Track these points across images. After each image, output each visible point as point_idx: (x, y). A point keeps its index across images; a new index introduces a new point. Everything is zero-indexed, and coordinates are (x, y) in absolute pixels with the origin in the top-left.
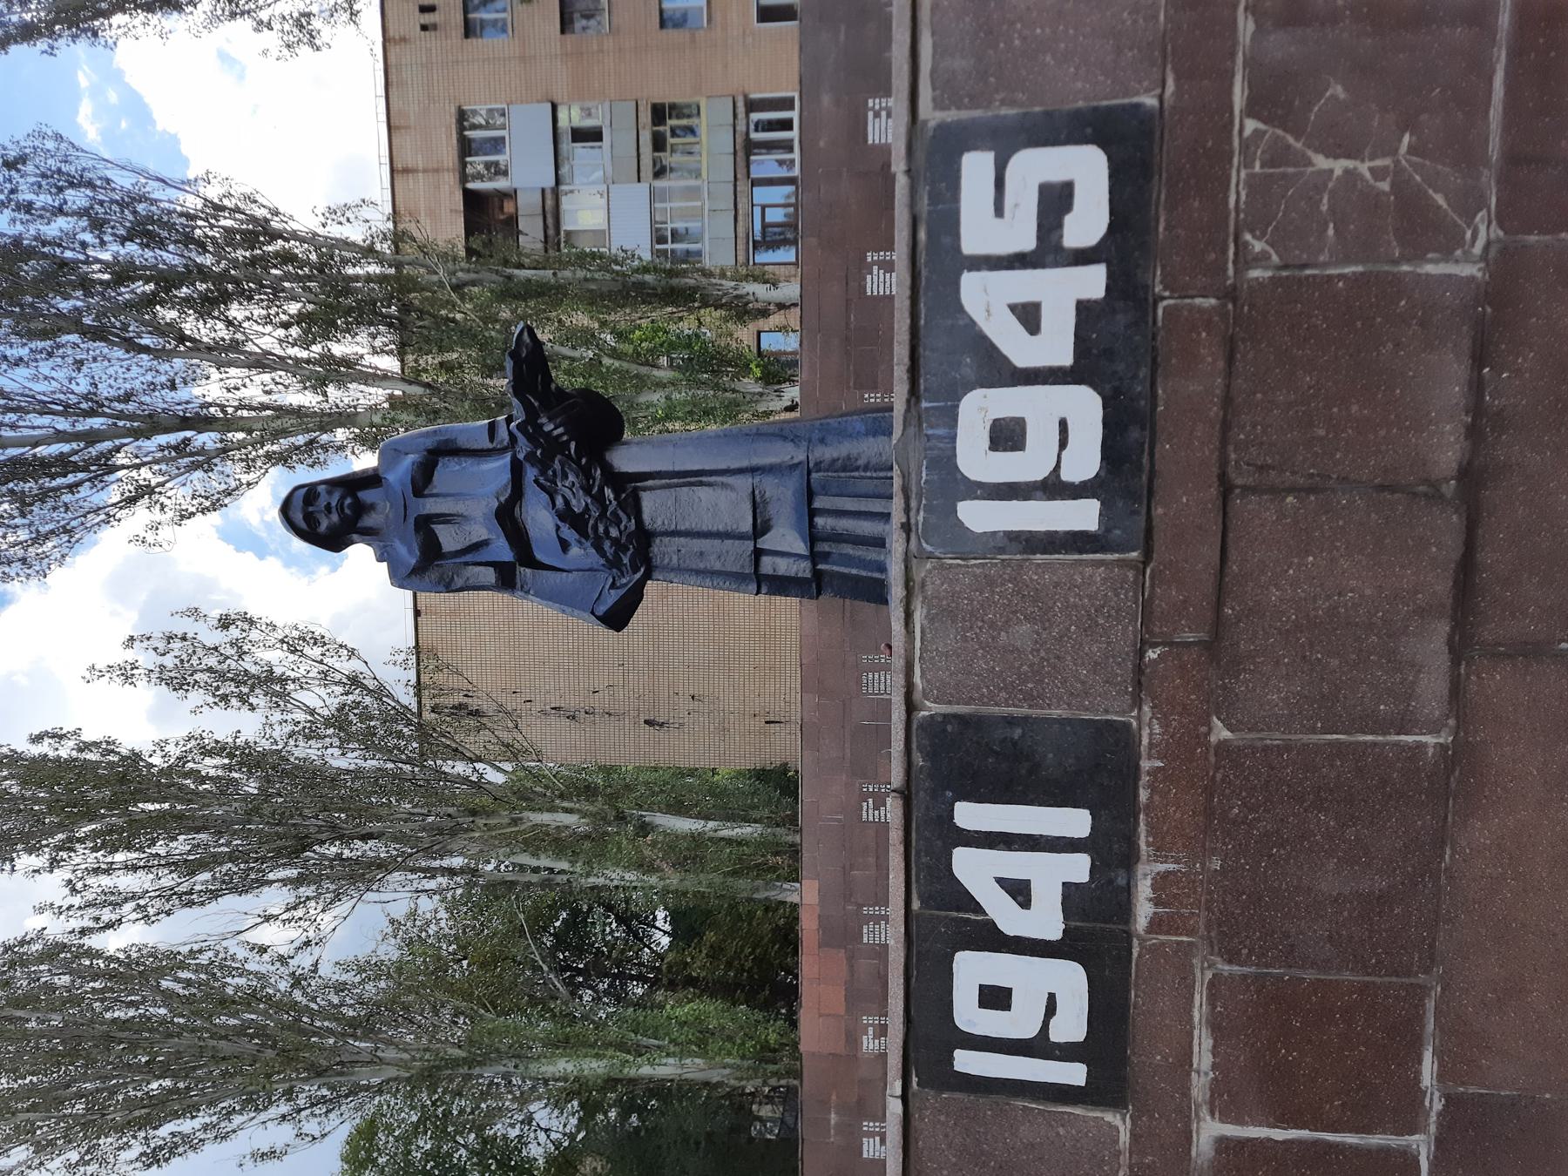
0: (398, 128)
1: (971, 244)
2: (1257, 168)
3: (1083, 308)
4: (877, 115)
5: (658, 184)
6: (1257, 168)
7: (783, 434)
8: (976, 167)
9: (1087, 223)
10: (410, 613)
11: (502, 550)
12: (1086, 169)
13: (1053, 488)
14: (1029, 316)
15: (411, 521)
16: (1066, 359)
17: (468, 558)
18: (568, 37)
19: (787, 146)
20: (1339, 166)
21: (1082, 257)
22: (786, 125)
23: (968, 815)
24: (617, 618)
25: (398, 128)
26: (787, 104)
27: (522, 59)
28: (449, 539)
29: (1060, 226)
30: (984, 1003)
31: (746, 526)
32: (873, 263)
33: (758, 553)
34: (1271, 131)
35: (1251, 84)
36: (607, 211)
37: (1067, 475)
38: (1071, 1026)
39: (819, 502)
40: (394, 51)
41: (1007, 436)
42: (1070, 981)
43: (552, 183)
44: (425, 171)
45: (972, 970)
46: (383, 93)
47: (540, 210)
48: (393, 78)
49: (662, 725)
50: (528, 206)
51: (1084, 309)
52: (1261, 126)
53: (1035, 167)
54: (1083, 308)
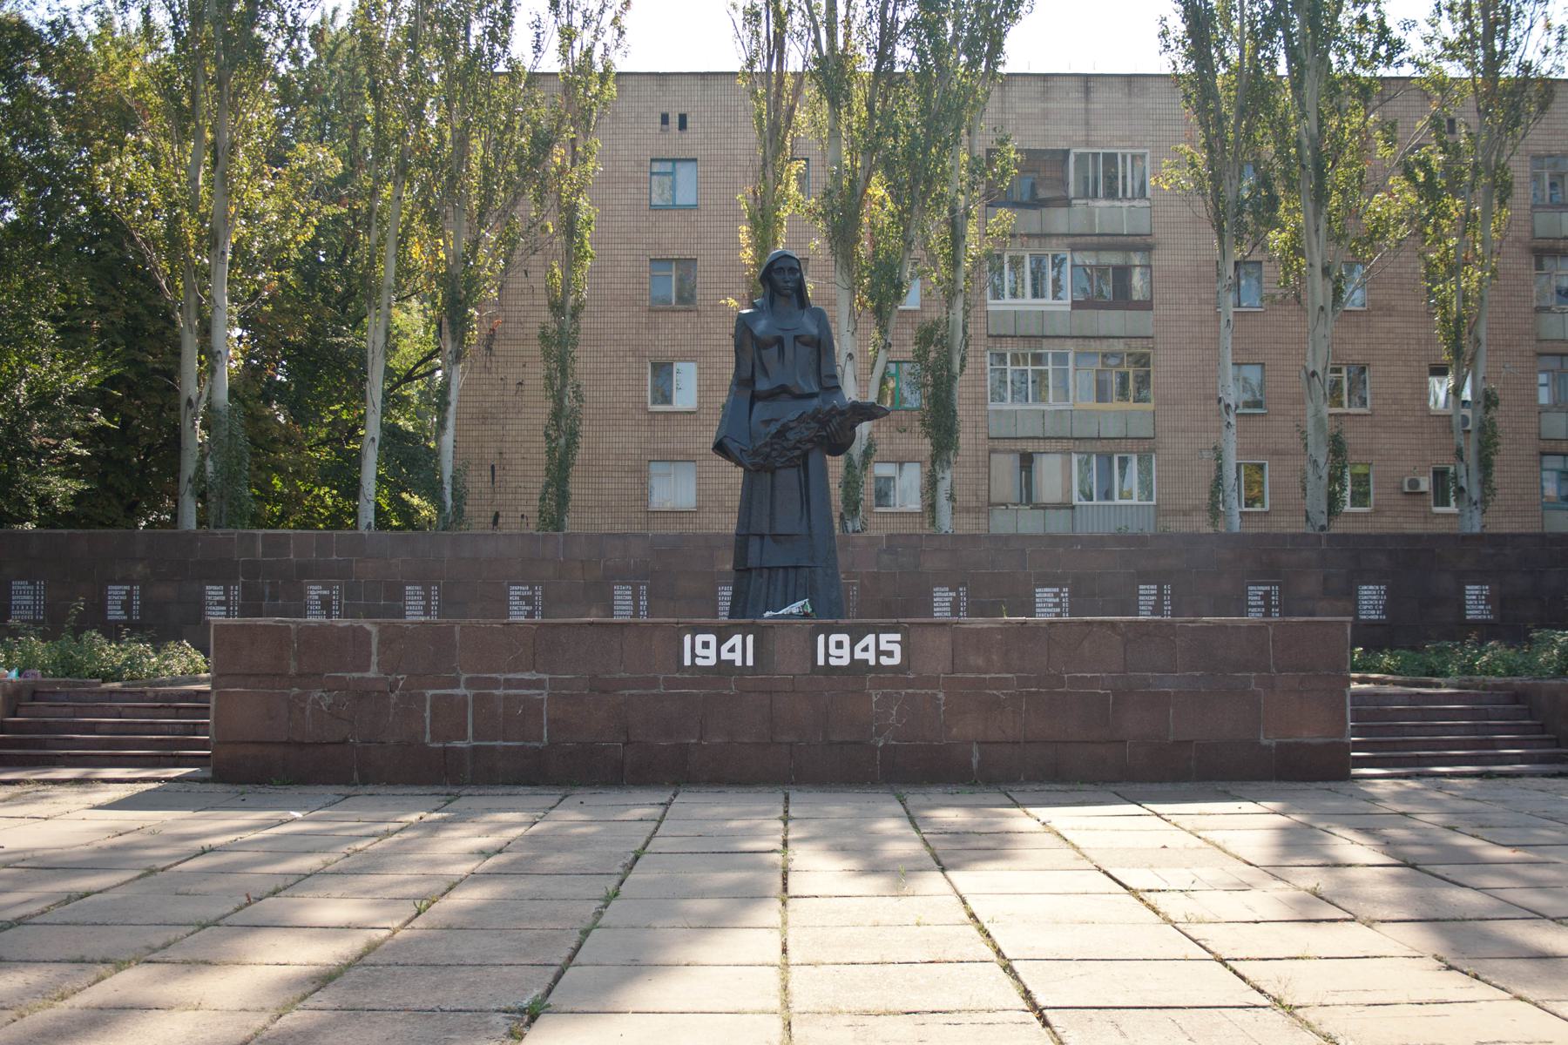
4: (1056, 595)
7: (768, 90)
8: (898, 637)
9: (884, 661)
11: (763, 385)
12: (896, 660)
13: (827, 655)
14: (866, 649)
15: (780, 333)
23: (750, 638)
24: (720, 448)
28: (771, 354)
31: (780, 529)
32: (958, 593)
33: (762, 536)
39: (792, 573)
41: (839, 645)
44: (1087, 110)
45: (712, 639)
47: (1046, 231)
49: (489, 347)
53: (897, 649)
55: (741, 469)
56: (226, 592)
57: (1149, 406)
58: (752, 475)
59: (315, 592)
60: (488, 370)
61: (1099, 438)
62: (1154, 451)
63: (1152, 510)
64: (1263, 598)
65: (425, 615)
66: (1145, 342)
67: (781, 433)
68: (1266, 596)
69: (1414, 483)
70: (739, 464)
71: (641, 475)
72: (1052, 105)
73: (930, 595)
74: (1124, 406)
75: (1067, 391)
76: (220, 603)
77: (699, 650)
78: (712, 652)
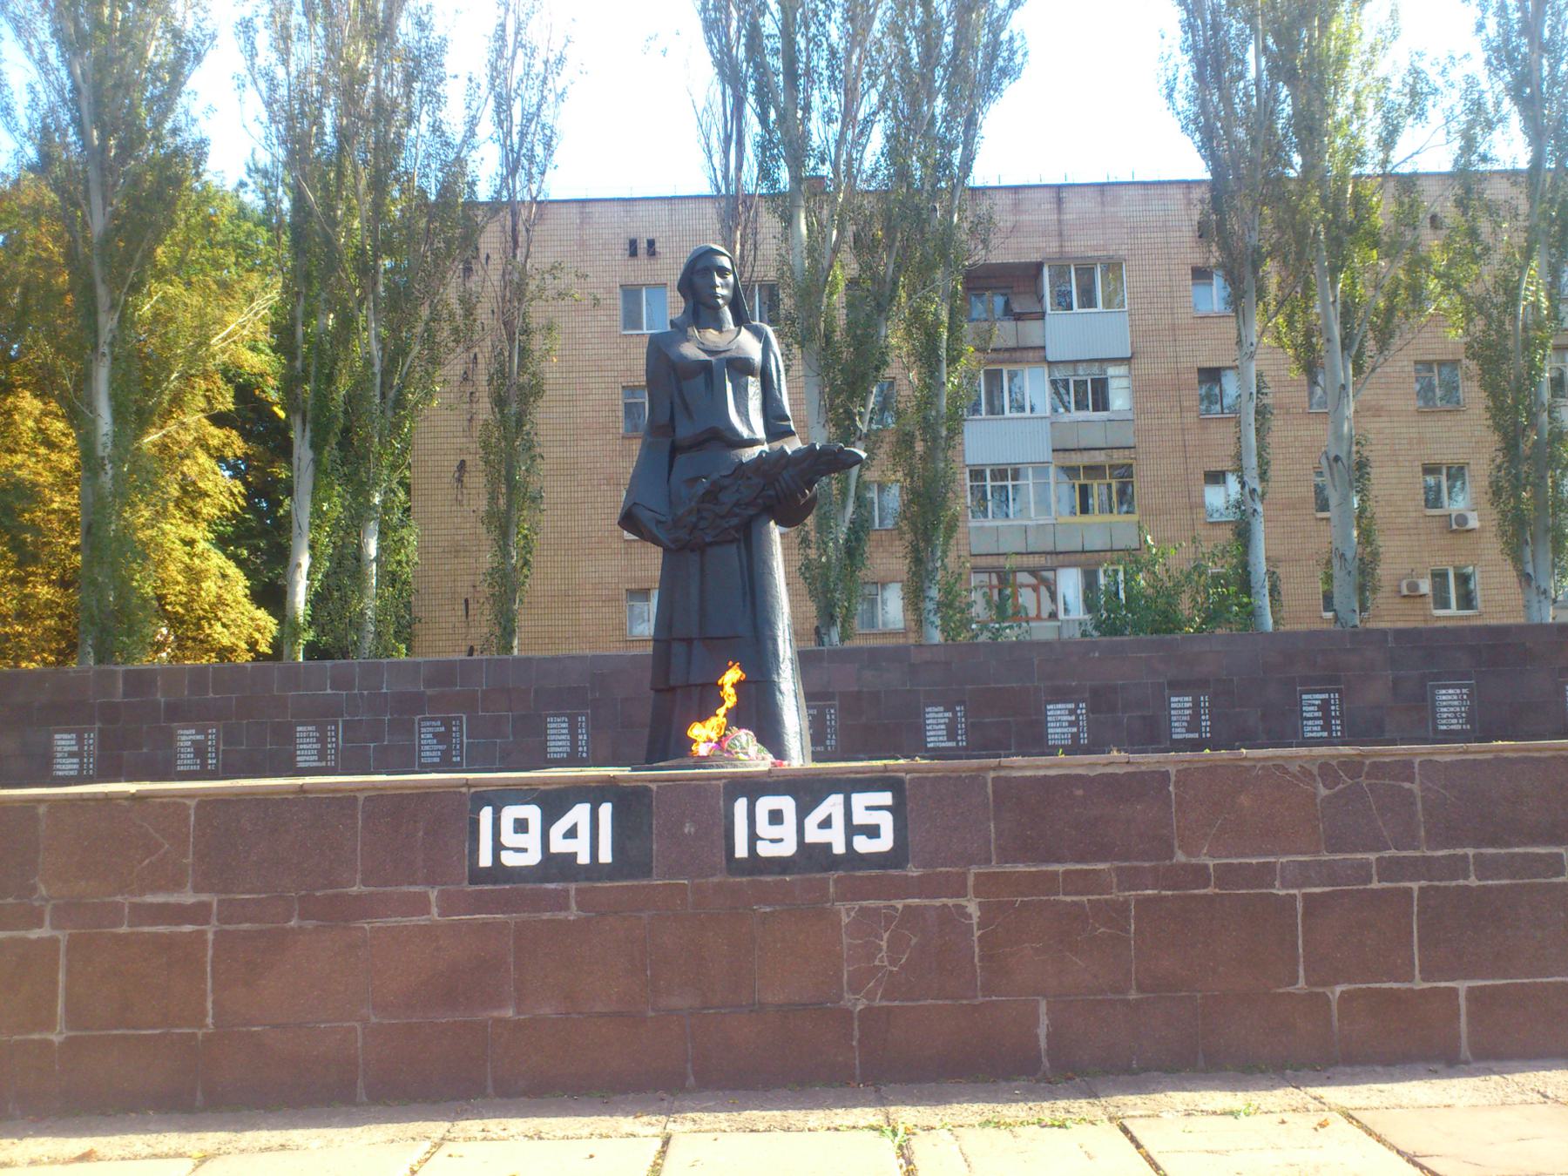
0: (1102, 194)
4: (1071, 712)
5: (1052, 470)
8: (886, 798)
9: (863, 845)
11: (685, 431)
12: (885, 843)
14: (826, 824)
17: (677, 400)
18: (1195, 376)
20: (884, 944)
21: (849, 843)
23: (606, 810)
24: (629, 520)
25: (1102, 194)
27: (1173, 328)
30: (516, 820)
32: (954, 713)
33: (689, 641)
36: (1015, 431)
37: (759, 843)
40: (1178, 193)
42: (533, 857)
43: (1050, 358)
44: (1060, 221)
45: (533, 813)
46: (1137, 179)
47: (1022, 344)
49: (460, 480)
50: (1031, 332)
51: (829, 846)
53: (886, 821)
56: (80, 741)
57: (1135, 518)
58: (674, 553)
59: (187, 737)
60: (460, 503)
61: (1083, 552)
64: (1320, 708)
66: (1127, 452)
67: (712, 495)
68: (1324, 706)
69: (1413, 587)
72: (1025, 218)
73: (920, 715)
74: (1106, 518)
75: (1049, 507)
76: (71, 755)
77: (508, 837)
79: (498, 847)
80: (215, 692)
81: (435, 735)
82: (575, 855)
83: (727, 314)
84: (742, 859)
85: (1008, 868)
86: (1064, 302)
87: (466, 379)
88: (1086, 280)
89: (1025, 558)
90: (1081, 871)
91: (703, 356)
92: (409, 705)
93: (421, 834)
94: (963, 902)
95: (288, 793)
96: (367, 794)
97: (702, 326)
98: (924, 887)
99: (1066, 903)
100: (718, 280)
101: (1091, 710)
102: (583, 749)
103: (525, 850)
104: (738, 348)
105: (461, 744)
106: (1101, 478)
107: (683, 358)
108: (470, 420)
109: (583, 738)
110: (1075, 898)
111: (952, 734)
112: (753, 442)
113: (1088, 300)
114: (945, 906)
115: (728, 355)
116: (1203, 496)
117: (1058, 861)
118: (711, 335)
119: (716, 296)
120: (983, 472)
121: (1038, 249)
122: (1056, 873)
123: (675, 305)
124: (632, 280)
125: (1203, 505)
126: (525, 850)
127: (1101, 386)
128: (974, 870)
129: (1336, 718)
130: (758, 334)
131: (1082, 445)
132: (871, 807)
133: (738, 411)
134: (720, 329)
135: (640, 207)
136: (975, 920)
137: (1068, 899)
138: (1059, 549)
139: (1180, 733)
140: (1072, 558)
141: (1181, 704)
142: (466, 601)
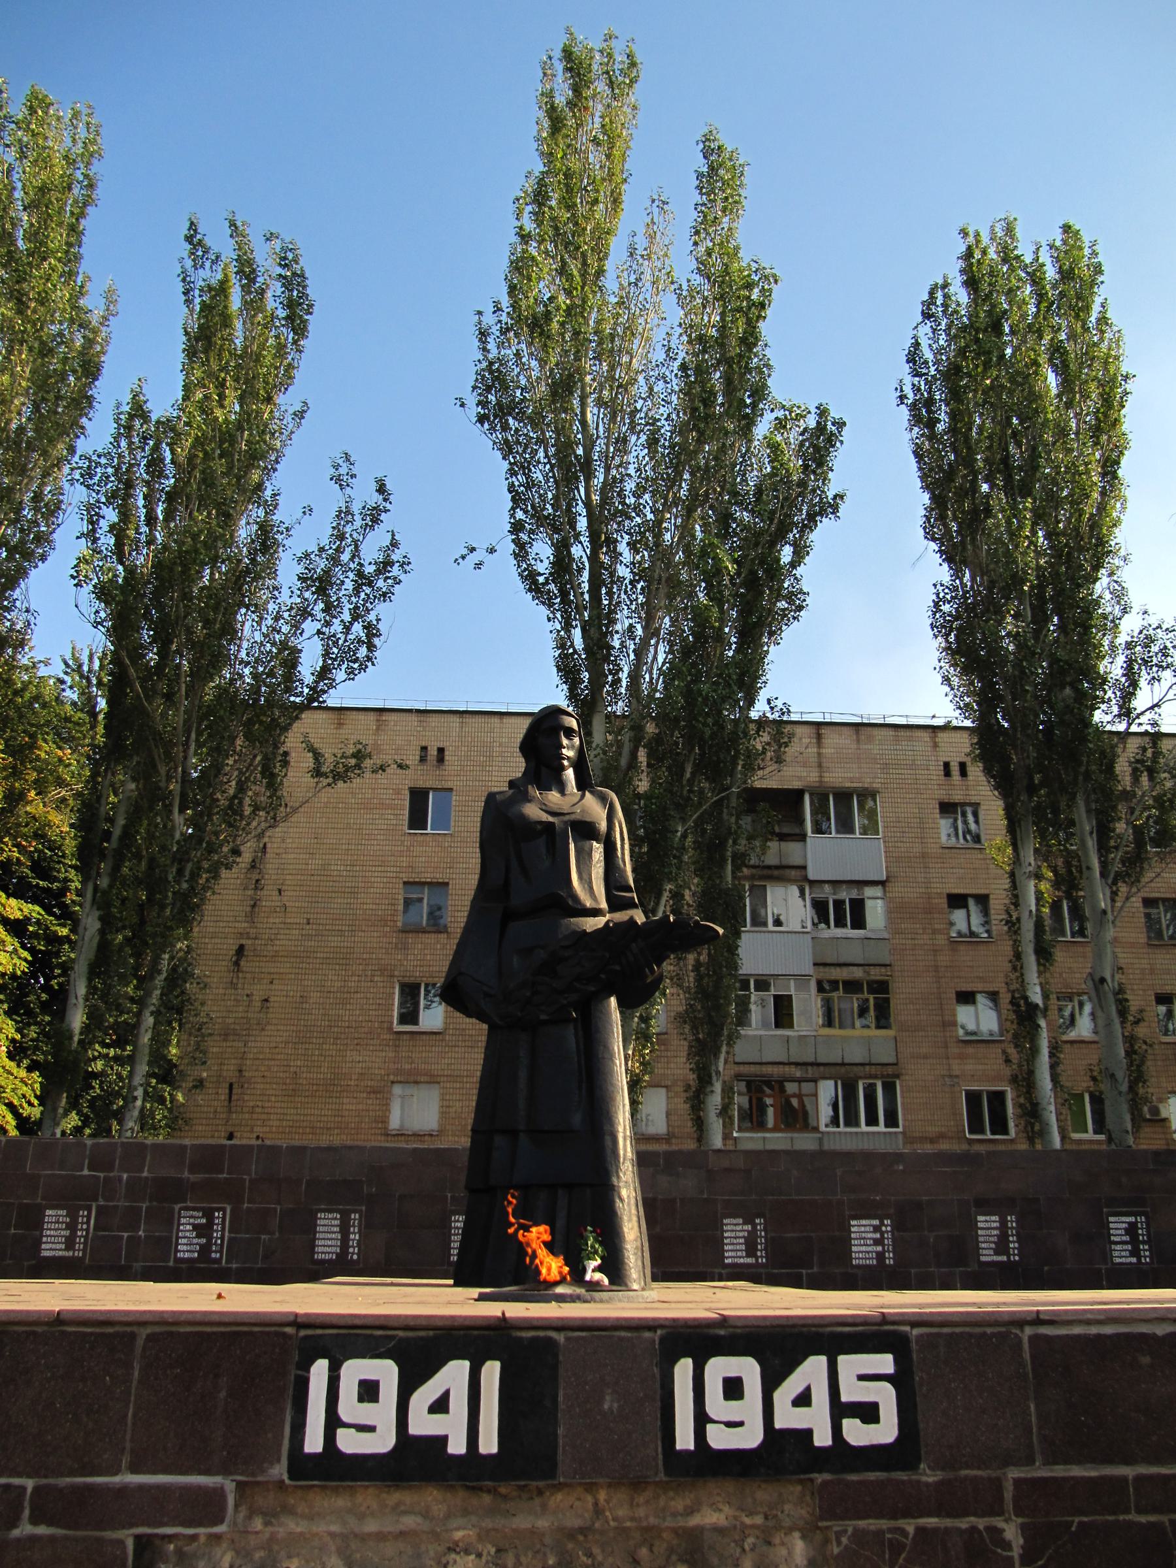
1: (842, 1359)
2: (888, 1536)
3: (809, 1433)
4: (876, 1229)
6: (888, 1536)
8: (885, 1363)
9: (856, 1433)
10: (379, 704)
12: (885, 1431)
13: (702, 1419)
14: (803, 1400)
16: (778, 1425)
19: (851, 1120)
22: (872, 1120)
23: (492, 1371)
25: (857, 733)
26: (891, 1120)
27: (924, 855)
29: (853, 1417)
30: (363, 1383)
32: (754, 1225)
34: (908, 1542)
35: (935, 1530)
38: (349, 1442)
41: (733, 1389)
42: (383, 1442)
44: (819, 754)
45: (386, 1372)
47: (784, 863)
48: (902, 733)
49: (237, 964)
50: (792, 852)
52: (911, 1536)
53: (886, 1396)
54: (809, 1433)
55: (485, 1026)
60: (233, 985)
62: (898, 1076)
63: (900, 1137)
65: (67, 1249)
66: (883, 970)
68: (1132, 1230)
70: (482, 1017)
71: (380, 1093)
73: (719, 1227)
78: (383, 1413)
79: (333, 1422)
80: (90, 1169)
81: (196, 1227)
82: (444, 1439)
83: (570, 774)
84: (686, 1452)
85: (1059, 1471)
86: (818, 830)
87: (253, 867)
88: (844, 806)
89: (787, 1068)
90: (1159, 1476)
91: (546, 817)
92: (168, 1194)
93: (223, 1394)
94: (998, 1522)
95: (36, 1323)
96: (149, 1330)
97: (544, 787)
98: (947, 1500)
99: (1140, 1524)
100: (565, 742)
101: (897, 1227)
102: (354, 1252)
103: (371, 1429)
104: (583, 811)
105: (222, 1238)
106: (865, 992)
107: (523, 817)
108: (254, 906)
109: (354, 1237)
110: (1152, 1518)
111: (751, 1250)
112: (596, 912)
113: (846, 826)
114: (973, 1529)
115: (573, 817)
116: (955, 1015)
117: (1128, 1461)
118: (554, 796)
119: (561, 757)
120: (748, 981)
121: (800, 778)
122: (1124, 1479)
123: (517, 766)
124: (421, 784)
125: (954, 1024)
126: (371, 1429)
127: (858, 906)
128: (1013, 1473)
129: (1144, 1242)
130: (603, 799)
131: (842, 961)
132: (865, 1374)
133: (580, 877)
134: (562, 791)
135: (434, 720)
136: (1016, 1553)
137: (1143, 1519)
138: (819, 1060)
139: (988, 1255)
140: (833, 1070)
141: (987, 1224)
142: (231, 1085)
